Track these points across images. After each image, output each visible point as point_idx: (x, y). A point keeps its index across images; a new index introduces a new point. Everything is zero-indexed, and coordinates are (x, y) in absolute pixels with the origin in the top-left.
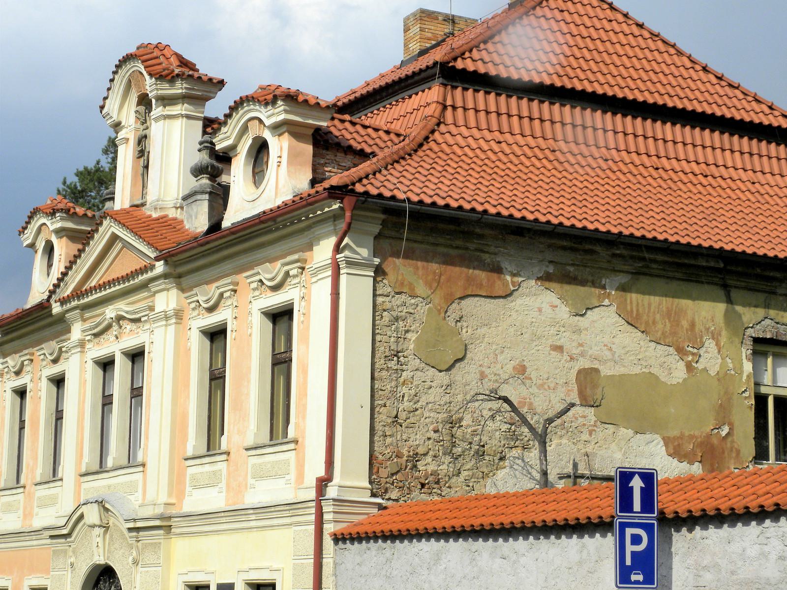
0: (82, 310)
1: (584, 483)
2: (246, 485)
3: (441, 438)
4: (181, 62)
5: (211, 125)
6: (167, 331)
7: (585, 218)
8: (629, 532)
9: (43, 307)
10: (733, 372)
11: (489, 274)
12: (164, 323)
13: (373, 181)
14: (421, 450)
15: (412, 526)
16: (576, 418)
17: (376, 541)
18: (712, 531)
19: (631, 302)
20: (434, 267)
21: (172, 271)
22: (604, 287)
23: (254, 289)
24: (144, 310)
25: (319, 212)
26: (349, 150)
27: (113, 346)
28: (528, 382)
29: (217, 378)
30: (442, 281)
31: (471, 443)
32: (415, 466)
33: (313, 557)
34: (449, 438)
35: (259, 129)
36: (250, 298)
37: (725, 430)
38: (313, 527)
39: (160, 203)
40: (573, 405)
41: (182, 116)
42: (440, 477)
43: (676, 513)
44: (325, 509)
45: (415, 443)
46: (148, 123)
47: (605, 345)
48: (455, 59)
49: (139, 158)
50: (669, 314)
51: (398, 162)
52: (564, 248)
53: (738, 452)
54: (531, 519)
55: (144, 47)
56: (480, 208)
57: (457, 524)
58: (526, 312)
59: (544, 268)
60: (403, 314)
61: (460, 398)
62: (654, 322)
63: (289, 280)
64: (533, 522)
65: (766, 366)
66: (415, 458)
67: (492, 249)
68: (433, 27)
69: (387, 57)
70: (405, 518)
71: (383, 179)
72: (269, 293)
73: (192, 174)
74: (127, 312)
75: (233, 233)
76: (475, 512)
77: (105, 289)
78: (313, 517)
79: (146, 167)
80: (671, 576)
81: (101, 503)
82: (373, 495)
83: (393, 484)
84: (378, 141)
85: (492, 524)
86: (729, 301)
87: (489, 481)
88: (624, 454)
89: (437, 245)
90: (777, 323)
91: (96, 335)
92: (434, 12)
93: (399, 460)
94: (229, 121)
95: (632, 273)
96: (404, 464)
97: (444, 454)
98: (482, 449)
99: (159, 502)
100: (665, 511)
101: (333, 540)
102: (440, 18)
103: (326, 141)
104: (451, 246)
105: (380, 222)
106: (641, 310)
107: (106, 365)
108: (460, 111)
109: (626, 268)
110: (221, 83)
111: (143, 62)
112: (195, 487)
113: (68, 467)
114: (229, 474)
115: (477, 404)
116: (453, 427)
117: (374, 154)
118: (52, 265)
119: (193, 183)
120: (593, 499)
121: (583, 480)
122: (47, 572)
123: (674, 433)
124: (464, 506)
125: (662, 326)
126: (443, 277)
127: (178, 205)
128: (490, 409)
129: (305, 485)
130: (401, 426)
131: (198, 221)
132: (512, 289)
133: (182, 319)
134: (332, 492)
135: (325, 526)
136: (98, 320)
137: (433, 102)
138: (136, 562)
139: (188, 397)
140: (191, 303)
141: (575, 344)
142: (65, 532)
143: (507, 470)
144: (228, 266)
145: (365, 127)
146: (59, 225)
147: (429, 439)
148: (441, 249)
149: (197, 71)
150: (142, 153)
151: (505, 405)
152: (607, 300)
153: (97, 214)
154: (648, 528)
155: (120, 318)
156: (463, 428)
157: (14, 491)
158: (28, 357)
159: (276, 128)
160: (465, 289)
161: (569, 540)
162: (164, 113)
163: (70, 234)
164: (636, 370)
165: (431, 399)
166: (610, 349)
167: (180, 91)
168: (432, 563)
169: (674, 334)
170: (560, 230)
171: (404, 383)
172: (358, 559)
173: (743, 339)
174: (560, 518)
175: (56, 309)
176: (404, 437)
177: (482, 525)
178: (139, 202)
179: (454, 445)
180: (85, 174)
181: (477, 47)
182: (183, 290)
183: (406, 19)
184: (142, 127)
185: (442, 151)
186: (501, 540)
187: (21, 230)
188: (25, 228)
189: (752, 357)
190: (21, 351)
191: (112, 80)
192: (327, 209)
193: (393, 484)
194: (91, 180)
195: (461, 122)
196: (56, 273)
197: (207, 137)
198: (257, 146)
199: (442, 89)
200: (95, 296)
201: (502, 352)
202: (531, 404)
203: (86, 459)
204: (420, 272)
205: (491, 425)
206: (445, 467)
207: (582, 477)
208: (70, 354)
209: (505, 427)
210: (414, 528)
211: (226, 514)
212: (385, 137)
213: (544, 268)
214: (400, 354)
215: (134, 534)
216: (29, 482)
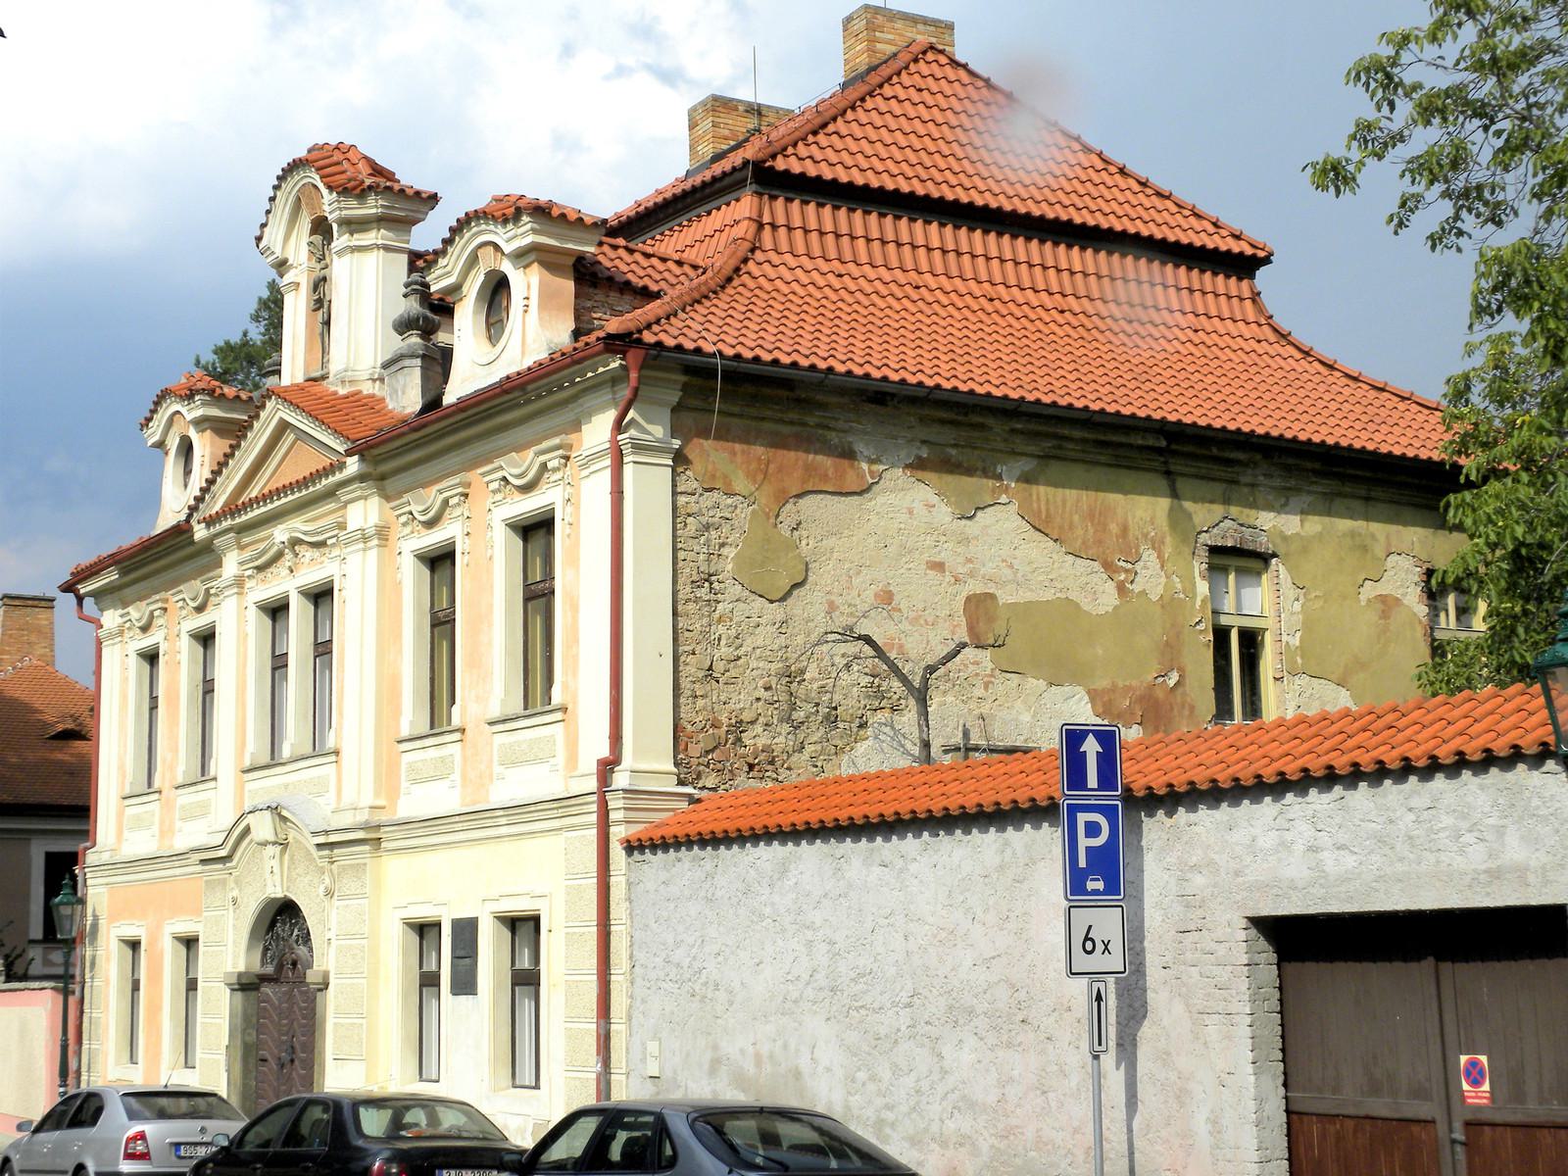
0: (238, 533)
2: (491, 776)
3: (775, 698)
4: (373, 169)
5: (420, 262)
7: (972, 379)
8: (1082, 818)
9: (181, 531)
10: (1182, 596)
11: (837, 460)
12: (361, 545)
13: (667, 327)
14: (746, 716)
15: (744, 825)
16: (966, 666)
18: (1203, 813)
19: (1038, 499)
20: (759, 450)
21: (371, 470)
22: (999, 478)
23: (494, 492)
25: (590, 375)
26: (626, 287)
28: (896, 615)
29: (442, 624)
30: (770, 471)
32: (739, 740)
33: (595, 875)
34: (788, 698)
35: (495, 259)
36: (488, 504)
38: (594, 831)
39: (349, 373)
40: (964, 645)
41: (378, 247)
42: (775, 754)
43: (1150, 788)
44: (611, 805)
45: (738, 706)
46: (328, 260)
47: (1003, 561)
48: (774, 157)
49: (315, 310)
50: (1091, 515)
52: (943, 422)
53: (1192, 708)
54: (925, 807)
55: (319, 149)
57: (813, 818)
58: (890, 515)
59: (915, 452)
60: (716, 519)
61: (800, 639)
62: (1071, 527)
63: (546, 475)
65: (1227, 587)
66: (739, 727)
67: (841, 424)
68: (731, 122)
69: (668, 165)
70: (730, 813)
71: (681, 325)
72: (517, 496)
73: (396, 330)
75: (463, 410)
76: (837, 800)
77: (272, 502)
78: (594, 818)
79: (327, 323)
80: (1143, 880)
81: (275, 810)
82: (681, 783)
83: (708, 766)
84: (666, 275)
85: (866, 817)
86: (1175, 494)
87: (845, 758)
88: (1033, 717)
89: (763, 419)
90: (1242, 525)
91: (260, 569)
93: (716, 731)
94: (450, 250)
95: (1039, 457)
96: (724, 736)
97: (781, 721)
98: (834, 712)
99: (361, 805)
100: (1132, 786)
101: (625, 849)
103: (594, 275)
104: (781, 421)
105: (679, 387)
106: (1052, 508)
107: (277, 611)
108: (782, 231)
109: (1031, 449)
110: (434, 199)
111: (318, 169)
112: (415, 782)
113: (224, 760)
114: (465, 759)
115: (825, 648)
116: (791, 683)
117: (657, 295)
118: (191, 471)
119: (397, 343)
120: (1016, 775)
121: (977, 754)
122: (198, 912)
123: (1102, 683)
124: (819, 793)
127: (376, 376)
128: (843, 655)
130: (718, 682)
131: (407, 397)
132: (871, 481)
133: (387, 540)
134: (620, 779)
135: (612, 829)
136: (262, 546)
137: (745, 219)
138: (329, 893)
139: (400, 651)
140: (400, 515)
141: (961, 560)
142: (223, 853)
143: (870, 742)
144: (455, 460)
145: (648, 256)
146: (199, 413)
147: (758, 699)
148: (767, 426)
149: (399, 181)
150: (320, 303)
151: (867, 647)
152: (1004, 496)
153: (256, 395)
154: (1109, 812)
155: (295, 542)
156: (806, 683)
158: (160, 605)
159: (521, 256)
160: (804, 482)
161: (984, 835)
162: (351, 244)
164: (1048, 595)
165: (760, 642)
166: (1011, 566)
167: (374, 211)
168: (776, 876)
169: (1100, 542)
170: (937, 395)
172: (664, 875)
173: (1195, 548)
174: (970, 802)
175: (200, 532)
177: (851, 819)
178: (317, 374)
179: (793, 707)
180: (226, 351)
181: (804, 139)
182: (388, 498)
183: (692, 112)
184: (319, 266)
185: (760, 288)
186: (879, 839)
187: (143, 421)
188: (149, 420)
189: (1206, 573)
190: (148, 596)
191: (272, 199)
192: (601, 370)
193: (708, 766)
194: (236, 359)
195: (784, 247)
196: (194, 490)
197: (415, 276)
198: (494, 283)
199: (756, 199)
200: (251, 515)
201: (859, 573)
202: (901, 646)
203: (250, 747)
204: (739, 459)
205: (845, 677)
206: (782, 740)
207: (976, 749)
208: (222, 597)
209: (865, 680)
210: (672, 834)
211: (463, 818)
212: (677, 270)
213: (915, 452)
214: (713, 578)
215: (326, 852)
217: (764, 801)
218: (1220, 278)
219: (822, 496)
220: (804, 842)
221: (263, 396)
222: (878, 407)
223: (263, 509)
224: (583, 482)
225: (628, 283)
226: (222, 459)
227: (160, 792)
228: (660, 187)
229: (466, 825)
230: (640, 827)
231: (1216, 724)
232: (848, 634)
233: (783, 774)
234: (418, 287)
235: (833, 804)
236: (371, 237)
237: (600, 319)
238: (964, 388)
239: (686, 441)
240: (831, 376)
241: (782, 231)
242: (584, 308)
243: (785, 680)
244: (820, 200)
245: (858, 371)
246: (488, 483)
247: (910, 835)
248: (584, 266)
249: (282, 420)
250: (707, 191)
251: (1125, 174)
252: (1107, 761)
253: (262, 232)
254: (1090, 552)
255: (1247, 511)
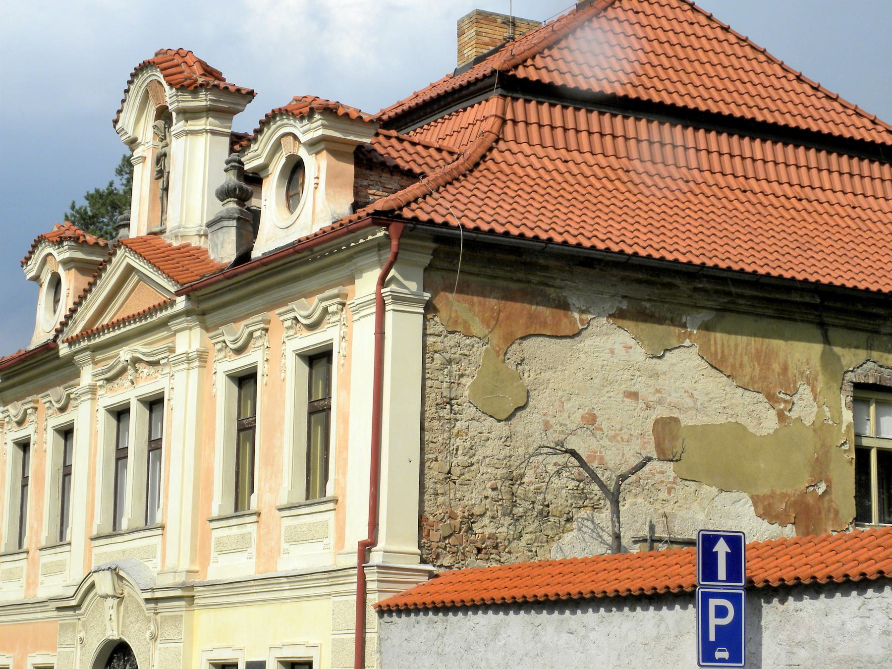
0: (93, 352)
1: (662, 548)
4: (205, 70)
6: (190, 375)
8: (713, 603)
9: (49, 348)
10: (830, 422)
11: (555, 310)
12: (186, 366)
13: (423, 205)
14: (477, 510)
15: (467, 597)
16: (653, 474)
17: (426, 614)
18: (807, 603)
19: (715, 343)
20: (492, 302)
21: (195, 307)
22: (684, 326)
23: (288, 328)
24: (164, 352)
25: (361, 241)
26: (395, 170)
27: (128, 392)
28: (598, 433)
29: (245, 429)
30: (501, 318)
31: (533, 503)
32: (471, 529)
34: (509, 497)
35: (294, 146)
36: (283, 338)
37: (822, 488)
38: (355, 597)
39: (181, 230)
40: (649, 459)
41: (206, 131)
42: (499, 540)
45: (470, 503)
47: (685, 392)
48: (516, 67)
49: (157, 179)
50: (758, 356)
51: (451, 183)
52: (639, 282)
53: (837, 513)
54: (601, 588)
56: (544, 236)
57: (518, 594)
58: (596, 355)
59: (617, 304)
60: (457, 356)
61: (521, 451)
62: (741, 366)
63: (327, 317)
64: (605, 592)
66: (470, 519)
67: (558, 282)
70: (459, 587)
72: (305, 333)
73: (218, 197)
74: (144, 354)
75: (264, 264)
76: (538, 580)
77: (119, 328)
79: (166, 189)
81: (114, 570)
82: (423, 561)
83: (445, 549)
84: (428, 160)
86: (827, 341)
88: (707, 516)
89: (496, 278)
90: (881, 366)
91: (109, 380)
92: (492, 14)
93: (452, 521)
94: (260, 138)
95: (717, 310)
96: (458, 526)
97: (504, 515)
99: (180, 569)
100: (753, 579)
102: (499, 21)
103: (370, 160)
105: (431, 252)
107: (120, 413)
108: (521, 126)
109: (710, 304)
110: (250, 95)
111: (162, 70)
112: (221, 552)
113: (77, 531)
114: (259, 537)
115: (540, 458)
116: (513, 485)
117: (423, 175)
118: (59, 301)
119: (220, 207)
121: (660, 545)
122: (54, 648)
123: (765, 491)
124: (526, 574)
125: (750, 369)
126: (502, 314)
127: (202, 233)
128: (555, 464)
129: (345, 550)
130: (455, 483)
131: (224, 250)
132: (581, 327)
134: (376, 557)
135: (369, 596)
136: (111, 362)
137: (491, 116)
138: (154, 638)
140: (216, 343)
141: (651, 390)
142: (73, 603)
145: (414, 144)
146: (67, 255)
147: (486, 497)
148: (500, 283)
149: (224, 80)
150: (161, 174)
151: (573, 459)
154: (735, 599)
155: (136, 361)
156: (525, 486)
157: (16, 557)
158: (32, 405)
159: (314, 145)
160: (527, 327)
163: (79, 265)
164: (721, 420)
166: (692, 396)
167: (204, 103)
168: (490, 638)
169: (764, 378)
170: (635, 260)
171: (457, 435)
172: (406, 634)
175: (64, 350)
176: (458, 496)
177: (546, 595)
179: (514, 504)
181: (541, 53)
182: (207, 329)
183: (460, 22)
184: (161, 144)
186: (567, 612)
187: (24, 260)
188: (28, 259)
190: (23, 398)
191: (127, 91)
192: (370, 238)
193: (445, 549)
194: (104, 205)
197: (234, 156)
198: (292, 166)
199: (501, 101)
201: (569, 399)
202: (602, 458)
203: (97, 521)
204: (476, 308)
205: (556, 481)
206: (504, 530)
207: (660, 540)
210: (470, 598)
211: (256, 583)
212: (436, 155)
214: (453, 402)
215: (152, 605)
216: (33, 546)
217: (485, 578)
218: (876, 165)
219: (541, 339)
220: (511, 612)
221: (114, 246)
222: (588, 270)
223: (112, 334)
224: (356, 325)
225: (397, 167)
226: (82, 294)
227: (27, 552)
228: (435, 81)
229: (258, 589)
230: (390, 595)
231: (856, 525)
232: (560, 448)
233: (505, 557)
234: (236, 164)
235: (535, 583)
236: (202, 124)
237: (374, 195)
238: (656, 255)
239: (434, 295)
240: (550, 245)
241: (521, 126)
242: (361, 186)
243: (508, 483)
244: (552, 102)
245: (572, 241)
246: (283, 321)
247: (590, 610)
248: (363, 154)
249: (128, 265)
250: (464, 92)
251: (801, 80)
252: (734, 560)
253: (118, 117)
254: (756, 386)
255: (886, 355)
